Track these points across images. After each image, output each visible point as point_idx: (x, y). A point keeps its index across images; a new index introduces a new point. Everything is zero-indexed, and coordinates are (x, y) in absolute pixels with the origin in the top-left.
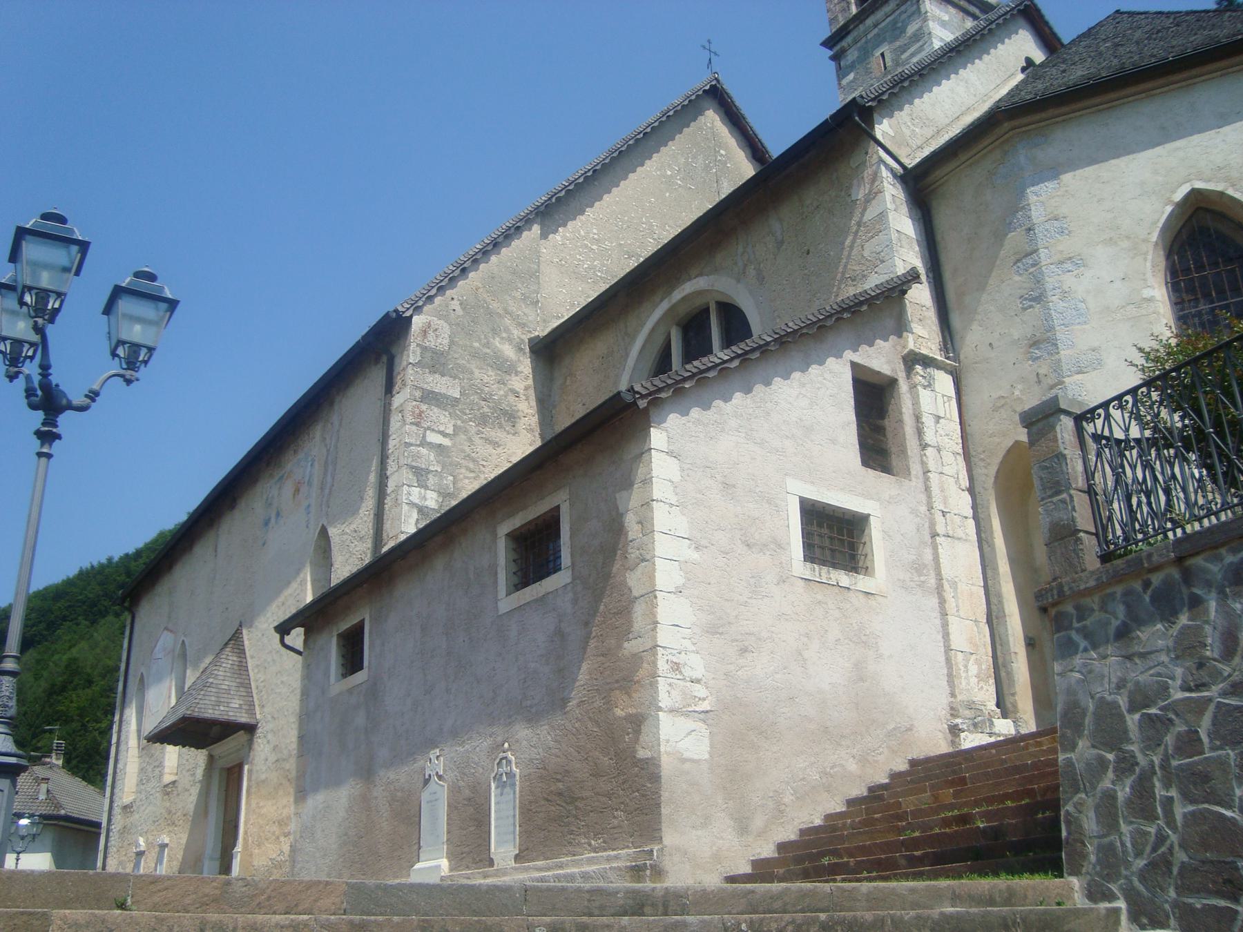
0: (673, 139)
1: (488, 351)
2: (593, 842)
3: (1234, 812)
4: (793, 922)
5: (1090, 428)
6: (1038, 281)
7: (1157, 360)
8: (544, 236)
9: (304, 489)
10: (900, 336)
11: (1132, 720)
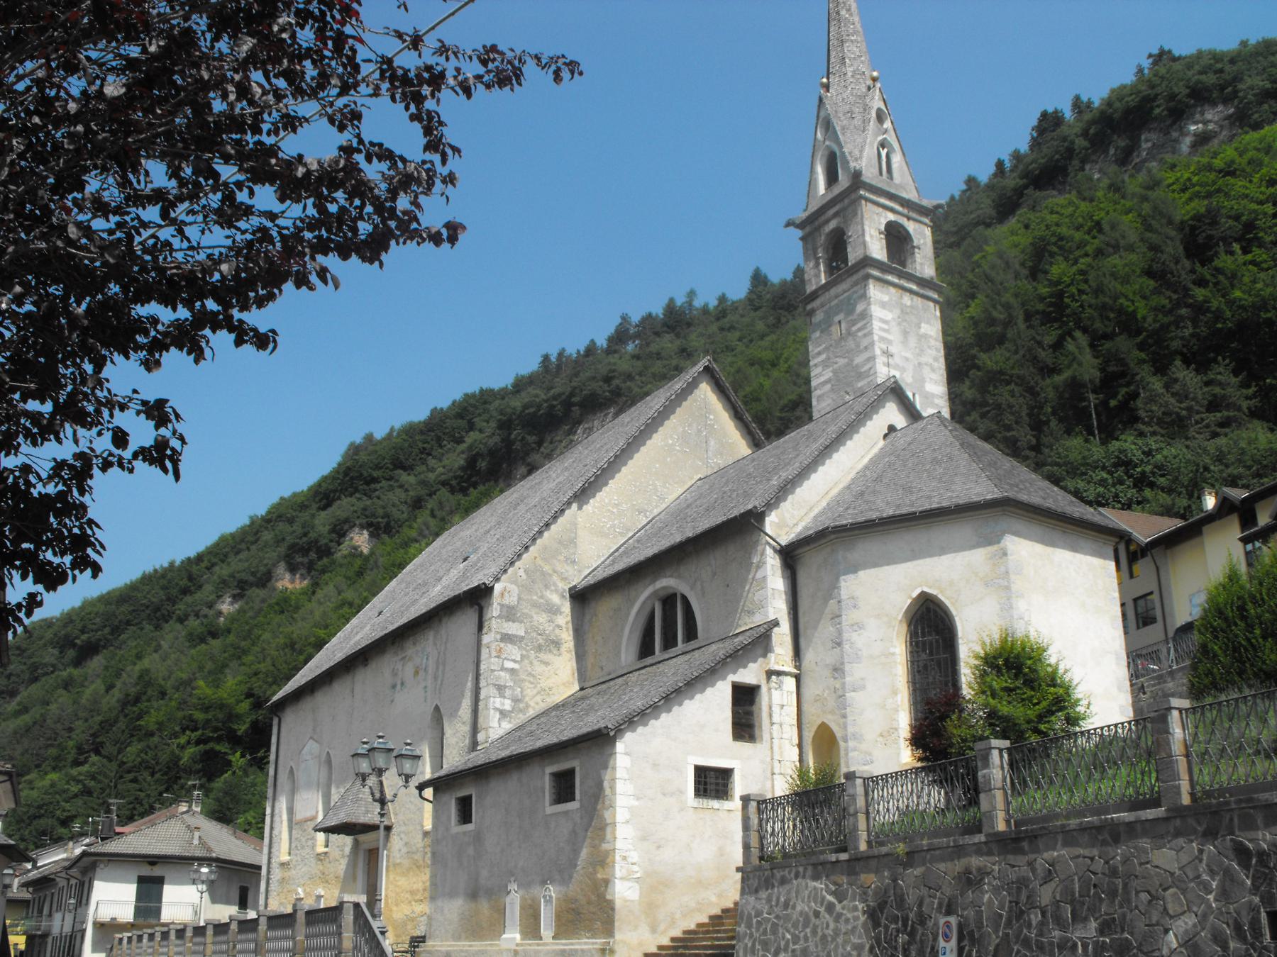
6: (840, 633)
8: (580, 508)
9: (422, 673)
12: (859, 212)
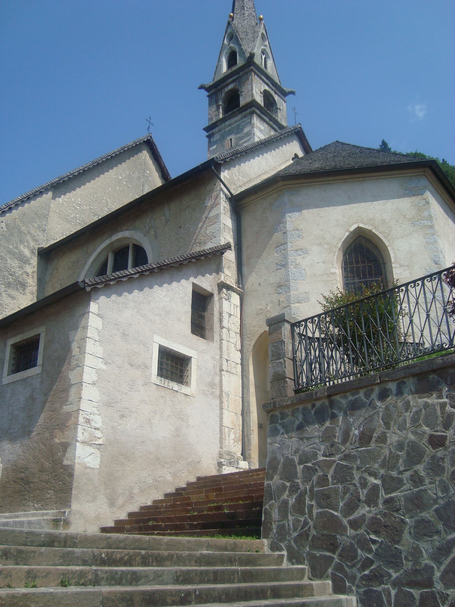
0: (125, 161)
1: (16, 251)
2: (36, 505)
3: (338, 513)
4: (128, 554)
5: (297, 330)
6: (285, 257)
7: (331, 303)
8: (54, 198)
10: (218, 274)
11: (300, 468)
12: (250, 78)
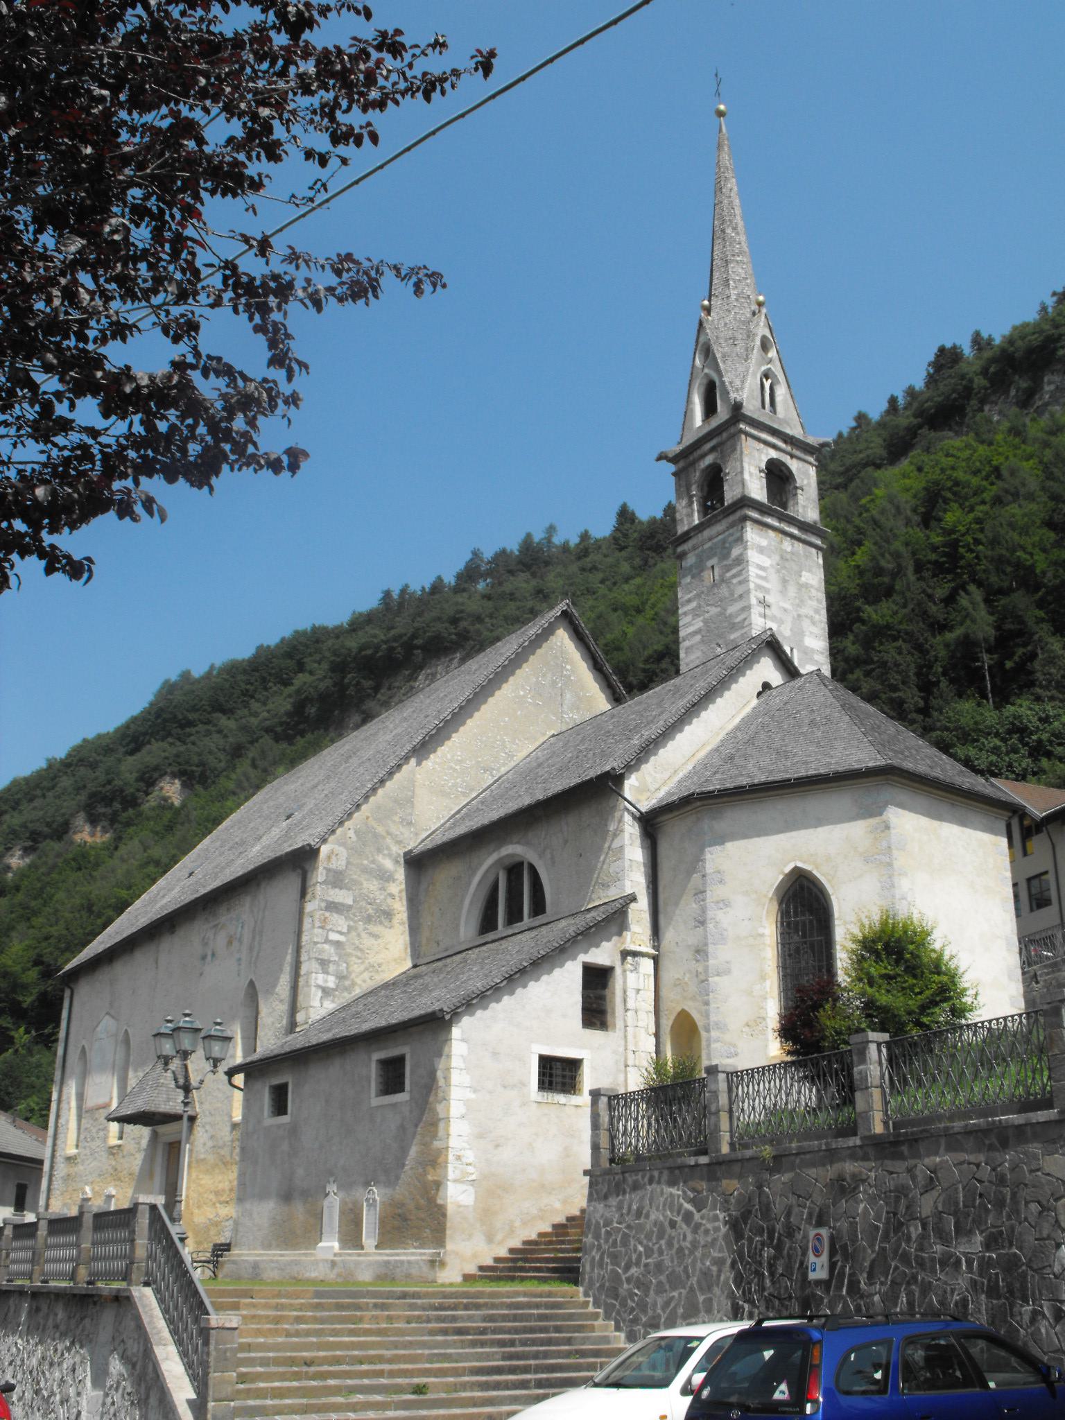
6: (704, 910)
8: (419, 764)
9: (236, 944)
